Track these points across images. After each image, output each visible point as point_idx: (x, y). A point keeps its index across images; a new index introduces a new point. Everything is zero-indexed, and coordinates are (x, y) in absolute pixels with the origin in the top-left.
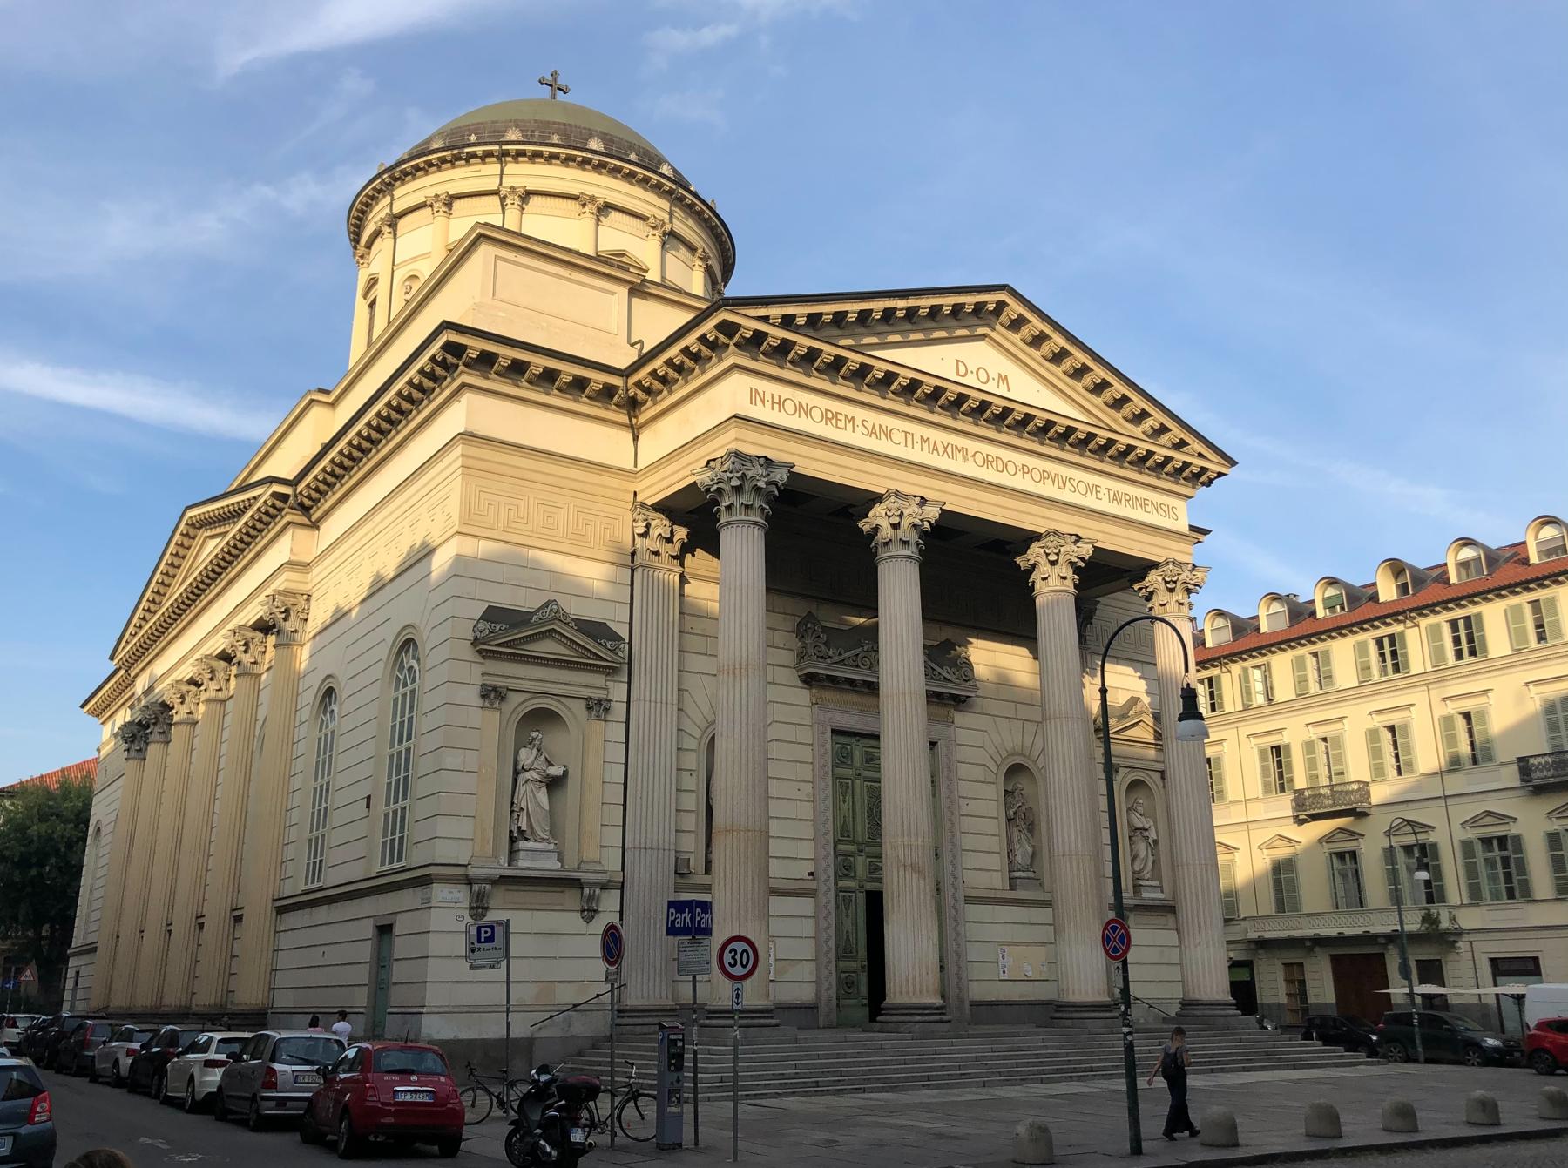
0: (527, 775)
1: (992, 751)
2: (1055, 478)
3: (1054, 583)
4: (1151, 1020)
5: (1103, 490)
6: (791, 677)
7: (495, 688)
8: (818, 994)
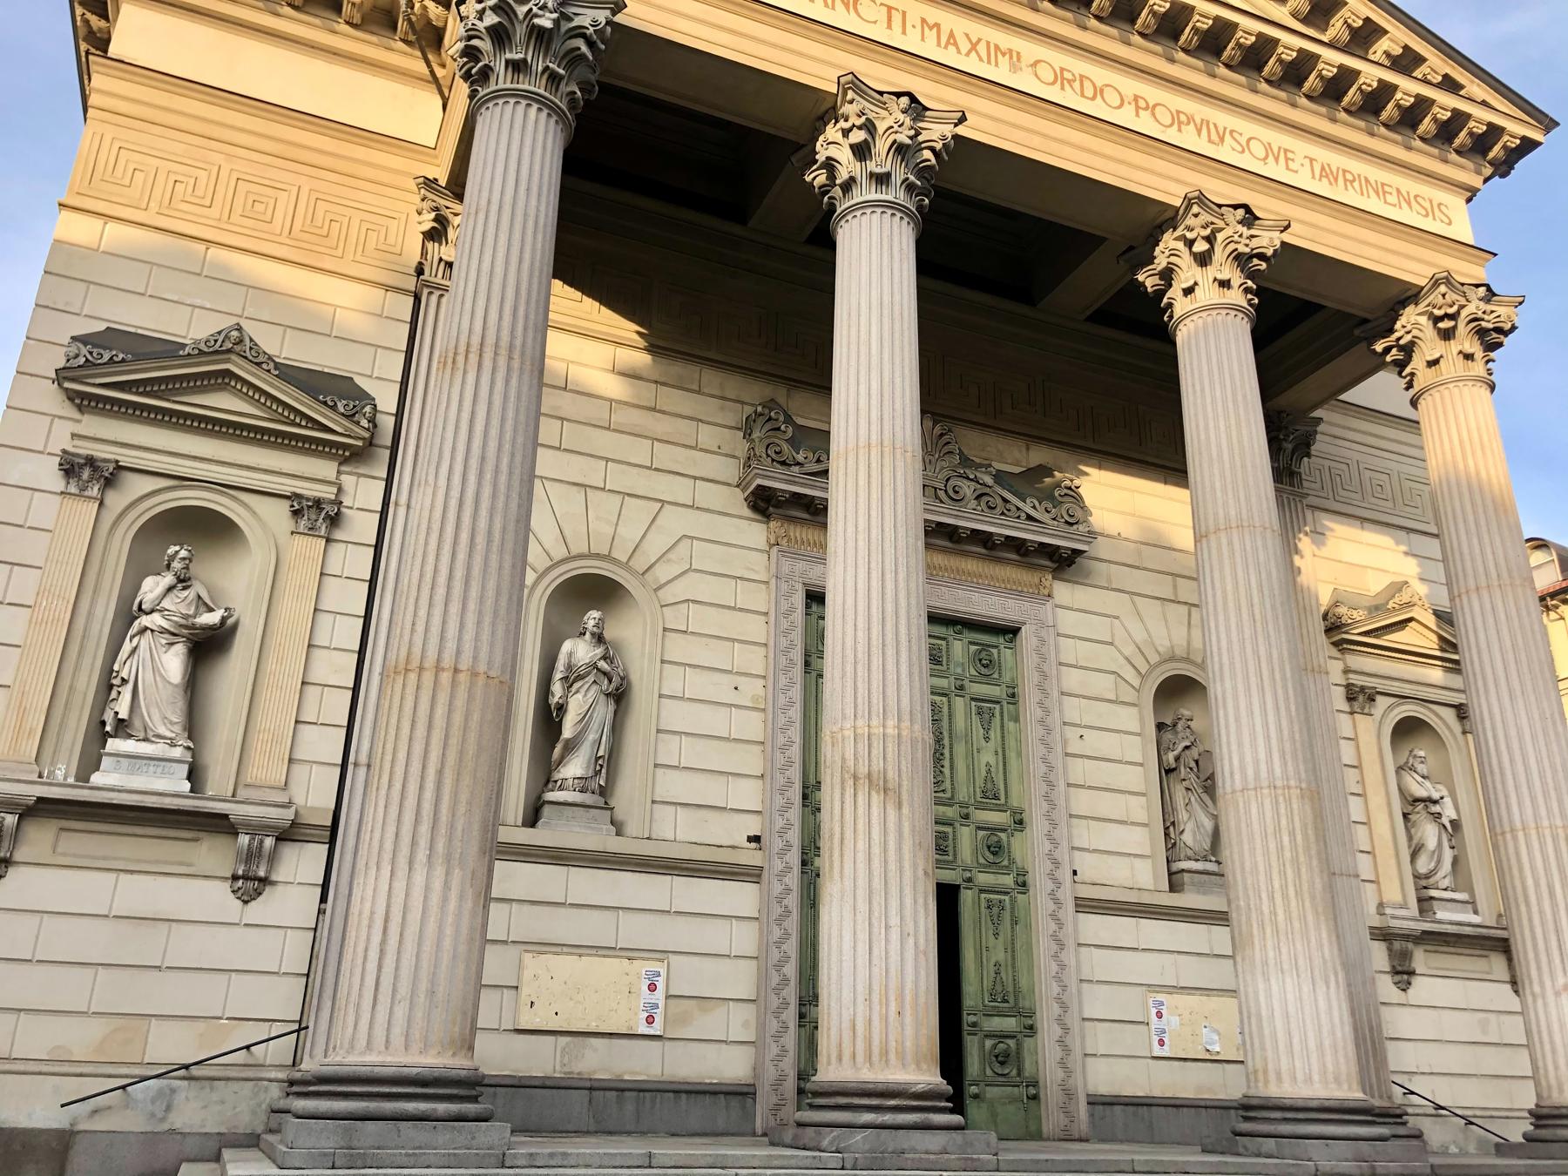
0: (145, 621)
1: (1129, 650)
2: (1201, 126)
3: (1207, 294)
4: (1472, 1149)
5: (1299, 159)
6: (736, 501)
7: (91, 461)
8: (756, 1069)
